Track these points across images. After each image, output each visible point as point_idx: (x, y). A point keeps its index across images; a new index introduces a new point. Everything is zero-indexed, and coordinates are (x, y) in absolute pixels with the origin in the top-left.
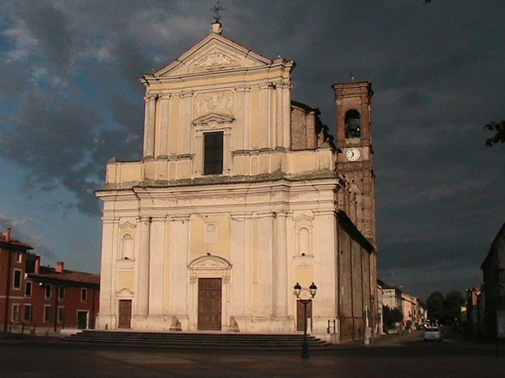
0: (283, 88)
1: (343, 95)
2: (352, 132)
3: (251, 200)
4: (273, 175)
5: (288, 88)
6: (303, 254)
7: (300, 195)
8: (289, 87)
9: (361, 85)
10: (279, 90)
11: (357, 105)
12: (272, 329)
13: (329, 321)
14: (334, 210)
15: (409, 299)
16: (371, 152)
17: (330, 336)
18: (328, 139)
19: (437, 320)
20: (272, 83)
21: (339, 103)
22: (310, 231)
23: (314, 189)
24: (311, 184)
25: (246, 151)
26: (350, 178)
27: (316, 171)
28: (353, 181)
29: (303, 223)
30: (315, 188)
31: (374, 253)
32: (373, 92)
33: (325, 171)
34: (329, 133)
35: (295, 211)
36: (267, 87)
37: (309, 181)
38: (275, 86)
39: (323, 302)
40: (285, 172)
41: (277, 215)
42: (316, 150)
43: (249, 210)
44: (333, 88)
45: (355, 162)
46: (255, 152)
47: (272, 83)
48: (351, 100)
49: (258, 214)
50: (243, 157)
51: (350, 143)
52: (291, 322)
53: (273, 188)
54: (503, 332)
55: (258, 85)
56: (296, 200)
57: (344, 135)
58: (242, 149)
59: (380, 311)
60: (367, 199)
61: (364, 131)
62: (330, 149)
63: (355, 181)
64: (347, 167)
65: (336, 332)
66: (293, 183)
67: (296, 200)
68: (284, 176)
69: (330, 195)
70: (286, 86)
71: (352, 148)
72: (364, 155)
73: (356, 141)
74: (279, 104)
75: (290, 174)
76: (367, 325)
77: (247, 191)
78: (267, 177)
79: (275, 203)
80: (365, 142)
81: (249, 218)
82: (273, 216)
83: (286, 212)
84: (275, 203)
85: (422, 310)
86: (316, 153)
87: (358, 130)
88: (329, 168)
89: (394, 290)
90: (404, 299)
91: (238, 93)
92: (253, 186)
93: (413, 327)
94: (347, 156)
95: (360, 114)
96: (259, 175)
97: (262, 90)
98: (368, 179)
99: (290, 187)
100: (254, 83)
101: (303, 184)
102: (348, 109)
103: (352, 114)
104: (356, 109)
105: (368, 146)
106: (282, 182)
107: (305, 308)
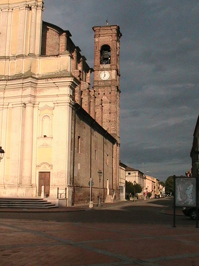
0: (37, 9)
1: (100, 35)
2: (105, 60)
3: (9, 93)
4: (25, 75)
5: (40, 9)
6: (45, 136)
7: (45, 90)
8: (41, 8)
9: (112, 28)
10: (33, 10)
11: (109, 42)
12: (18, 195)
13: (58, 188)
14: (69, 101)
15: (150, 179)
16: (118, 74)
17: (58, 200)
18: (81, 59)
19: (171, 193)
20: (28, 5)
21: (97, 40)
22: (51, 118)
23: (55, 86)
24: (53, 82)
25: (7, 57)
26: (103, 91)
27: (58, 72)
28: (104, 94)
29: (47, 112)
30: (56, 85)
31: (117, 144)
32: (121, 34)
33: (64, 72)
34: (82, 53)
35: (40, 103)
36: (25, 8)
37: (51, 80)
38: (31, 7)
39: (58, 174)
40: (34, 73)
41: (27, 105)
42: (58, 56)
43: (6, 101)
44: (93, 29)
45: (106, 80)
46: (13, 58)
47: (28, 5)
48: (107, 38)
49: (12, 105)
50: (4, 61)
51: (103, 68)
52: (33, 189)
53: (24, 84)
54: (181, 200)
55: (18, 7)
56: (42, 94)
57: (99, 62)
58: (4, 56)
59: (123, 185)
60: (113, 106)
61: (113, 59)
62: (68, 55)
63: (105, 94)
64: (100, 84)
65: (67, 198)
66: (39, 80)
67: (42, 94)
68: (33, 76)
69: (67, 91)
70: (39, 8)
71: (105, 71)
72: (112, 76)
73: (108, 66)
74: (33, 21)
75: (38, 74)
76: (108, 193)
77: (5, 87)
78: (20, 76)
79: (26, 96)
80: (113, 67)
81: (6, 108)
82: (23, 106)
83: (33, 103)
84: (26, 96)
85: (161, 186)
86: (58, 58)
87: (109, 59)
88: (67, 70)
89: (138, 172)
90: (145, 178)
91: (3, 12)
92: (9, 83)
93: (153, 196)
94: (101, 77)
95: (111, 48)
96: (15, 75)
97: (21, 11)
98: (114, 92)
99: (37, 84)
100: (16, 5)
101: (47, 82)
102: (103, 44)
103: (106, 48)
104: (108, 44)
105: (115, 70)
106: (30, 80)
107: (45, 178)
